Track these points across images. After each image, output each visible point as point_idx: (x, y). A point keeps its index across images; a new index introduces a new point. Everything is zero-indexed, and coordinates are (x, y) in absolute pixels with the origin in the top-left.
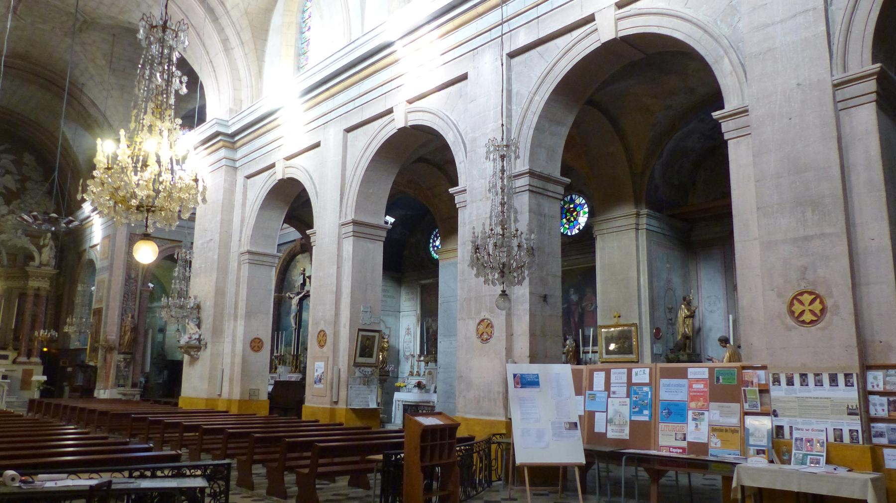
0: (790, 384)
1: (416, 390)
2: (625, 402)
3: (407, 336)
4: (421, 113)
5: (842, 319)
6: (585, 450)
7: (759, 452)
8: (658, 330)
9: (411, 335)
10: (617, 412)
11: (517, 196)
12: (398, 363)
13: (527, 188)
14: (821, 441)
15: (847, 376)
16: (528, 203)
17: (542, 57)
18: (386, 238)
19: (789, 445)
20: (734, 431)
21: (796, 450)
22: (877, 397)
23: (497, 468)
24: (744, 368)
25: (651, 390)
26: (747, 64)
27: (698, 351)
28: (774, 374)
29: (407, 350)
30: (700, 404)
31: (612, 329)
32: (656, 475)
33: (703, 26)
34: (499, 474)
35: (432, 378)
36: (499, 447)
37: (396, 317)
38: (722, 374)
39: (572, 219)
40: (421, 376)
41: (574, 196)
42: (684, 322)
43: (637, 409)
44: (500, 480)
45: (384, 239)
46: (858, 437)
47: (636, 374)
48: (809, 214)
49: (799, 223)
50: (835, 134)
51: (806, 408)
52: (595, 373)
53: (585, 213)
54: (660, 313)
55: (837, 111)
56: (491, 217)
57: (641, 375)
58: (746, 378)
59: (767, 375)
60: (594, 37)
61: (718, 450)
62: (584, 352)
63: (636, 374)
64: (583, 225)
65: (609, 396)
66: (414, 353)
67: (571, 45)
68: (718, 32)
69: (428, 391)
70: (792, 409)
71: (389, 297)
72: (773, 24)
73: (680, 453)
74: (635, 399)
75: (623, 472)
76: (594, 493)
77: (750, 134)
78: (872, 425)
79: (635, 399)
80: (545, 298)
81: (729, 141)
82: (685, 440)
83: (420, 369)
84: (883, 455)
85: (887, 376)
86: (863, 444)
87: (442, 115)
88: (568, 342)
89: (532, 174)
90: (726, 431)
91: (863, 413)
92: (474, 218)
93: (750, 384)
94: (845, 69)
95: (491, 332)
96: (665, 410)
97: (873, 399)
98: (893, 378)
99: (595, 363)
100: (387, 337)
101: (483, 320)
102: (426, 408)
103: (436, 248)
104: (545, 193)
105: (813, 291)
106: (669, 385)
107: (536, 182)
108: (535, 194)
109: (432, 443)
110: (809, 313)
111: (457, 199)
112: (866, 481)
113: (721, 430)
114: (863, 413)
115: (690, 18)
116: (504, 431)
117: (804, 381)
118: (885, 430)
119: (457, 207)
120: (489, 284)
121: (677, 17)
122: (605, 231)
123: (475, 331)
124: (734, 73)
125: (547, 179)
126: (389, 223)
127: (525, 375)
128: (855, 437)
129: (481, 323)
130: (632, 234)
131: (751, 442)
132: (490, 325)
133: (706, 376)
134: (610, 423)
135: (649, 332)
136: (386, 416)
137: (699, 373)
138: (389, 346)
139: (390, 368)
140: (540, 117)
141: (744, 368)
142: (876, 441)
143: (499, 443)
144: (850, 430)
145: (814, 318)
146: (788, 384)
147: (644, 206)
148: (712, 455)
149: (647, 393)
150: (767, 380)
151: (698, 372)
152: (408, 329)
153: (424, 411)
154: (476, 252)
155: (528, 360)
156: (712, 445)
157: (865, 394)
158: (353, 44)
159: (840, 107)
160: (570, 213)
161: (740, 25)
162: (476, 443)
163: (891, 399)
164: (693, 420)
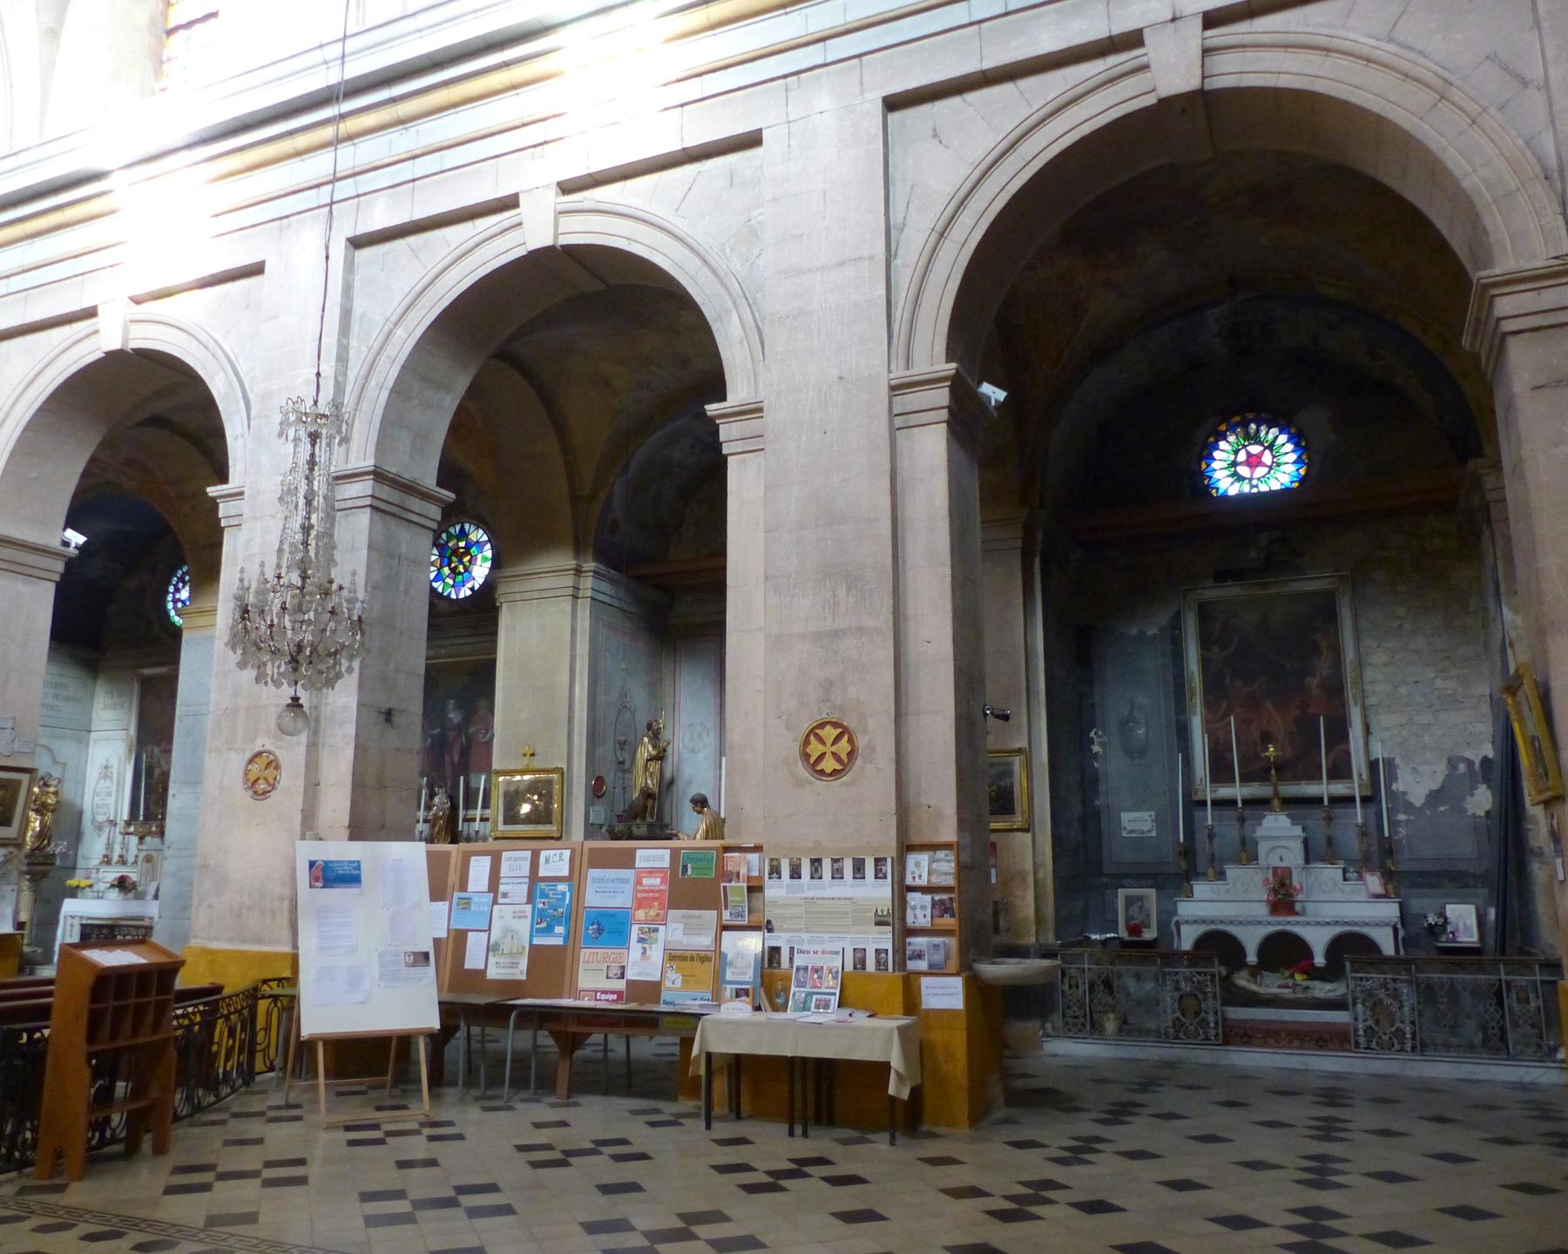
0: (881, 875)
1: (114, 894)
2: (524, 912)
3: (102, 781)
4: (153, 326)
5: (877, 768)
6: (441, 1003)
7: (739, 994)
8: (600, 781)
9: (112, 780)
10: (509, 932)
11: (347, 515)
12: (77, 836)
13: (368, 501)
14: (834, 970)
15: (879, 861)
16: (366, 532)
17: (417, 257)
18: (62, 576)
19: (786, 979)
20: (705, 960)
21: (797, 987)
22: (918, 895)
23: (268, 1046)
24: (727, 849)
25: (570, 890)
26: (765, 330)
27: (667, 820)
28: (772, 860)
29: (99, 810)
30: (652, 913)
31: (518, 778)
32: (567, 1043)
33: (703, 253)
34: (272, 1058)
35: (153, 870)
36: (276, 1005)
37: (79, 741)
38: (692, 860)
39: (461, 569)
40: (129, 864)
41: (467, 526)
42: (646, 768)
43: (544, 925)
44: (271, 1069)
45: (57, 578)
46: (887, 962)
47: (547, 861)
48: (841, 593)
49: (827, 608)
50: (887, 467)
51: (818, 916)
52: (473, 859)
53: (485, 559)
54: (607, 751)
55: (893, 431)
56: (280, 550)
57: (556, 862)
58: (729, 868)
59: (761, 861)
60: (513, 238)
61: (678, 994)
62: (466, 820)
63: (547, 861)
64: (481, 581)
65: (495, 902)
66: (116, 816)
67: (471, 243)
68: (725, 267)
69: (140, 896)
70: (795, 918)
71: (68, 699)
72: (810, 270)
73: (613, 1001)
74: (541, 906)
75: (512, 1040)
76: (454, 1084)
77: (763, 449)
78: (908, 940)
79: (541, 906)
80: (388, 715)
81: (730, 458)
82: (623, 978)
83: (127, 851)
84: (919, 988)
85: (934, 861)
86: (894, 971)
87: (203, 337)
88: (436, 800)
89: (378, 475)
90: (692, 959)
91: (896, 921)
92: (256, 551)
93: (734, 878)
94: (908, 364)
95: (275, 778)
96: (592, 924)
97: (914, 899)
98: (940, 864)
99: (485, 839)
100: (55, 783)
101: (259, 754)
102: (134, 932)
103: (180, 605)
104: (404, 514)
105: (839, 721)
106: (601, 880)
107: (386, 492)
108: (384, 515)
109: (117, 1004)
110: (831, 758)
111: (224, 509)
112: (891, 1031)
113: (683, 958)
114: (896, 921)
115: (682, 235)
116: (287, 974)
117: (816, 870)
118: (924, 948)
119: (222, 525)
120: (266, 684)
121: (662, 228)
122: (518, 597)
123: (241, 773)
124: (745, 343)
125: (410, 488)
126: (73, 545)
127: (332, 862)
128: (882, 961)
129: (256, 760)
130: (566, 605)
131: (729, 977)
132: (274, 764)
133: (666, 863)
134: (494, 951)
135: (584, 784)
136: (40, 950)
137: (654, 858)
138: (58, 802)
139: (58, 848)
140: (404, 368)
141: (727, 849)
142: (912, 965)
143: (275, 998)
144: (876, 950)
145: (839, 767)
146: (792, 877)
147: (590, 557)
148: (665, 1003)
149: (564, 894)
150: (761, 870)
151: (653, 856)
152: (106, 767)
153: (128, 938)
154: (243, 619)
155: (346, 833)
156: (667, 984)
157: (903, 890)
158: (13, 158)
159: (899, 424)
160: (457, 557)
161: (761, 262)
162: (223, 999)
163: (937, 897)
164: (638, 942)
